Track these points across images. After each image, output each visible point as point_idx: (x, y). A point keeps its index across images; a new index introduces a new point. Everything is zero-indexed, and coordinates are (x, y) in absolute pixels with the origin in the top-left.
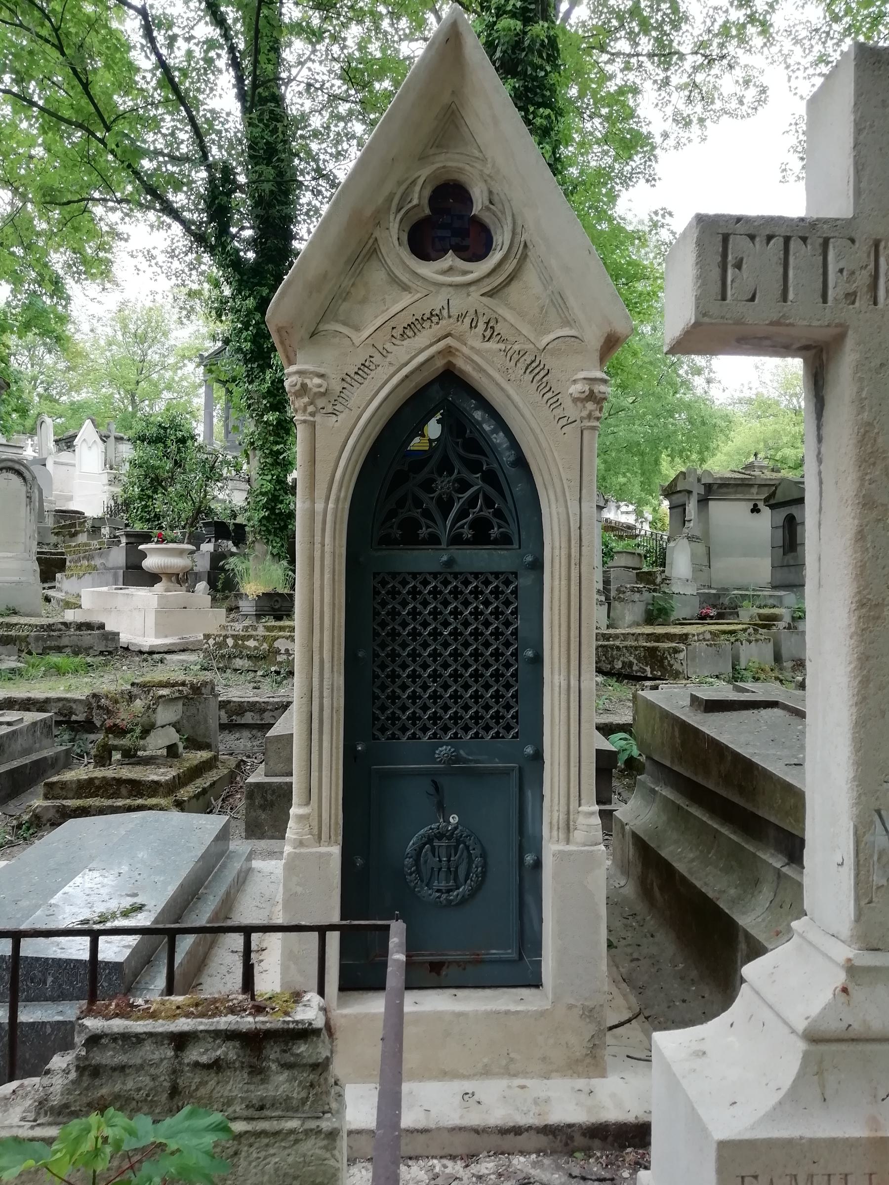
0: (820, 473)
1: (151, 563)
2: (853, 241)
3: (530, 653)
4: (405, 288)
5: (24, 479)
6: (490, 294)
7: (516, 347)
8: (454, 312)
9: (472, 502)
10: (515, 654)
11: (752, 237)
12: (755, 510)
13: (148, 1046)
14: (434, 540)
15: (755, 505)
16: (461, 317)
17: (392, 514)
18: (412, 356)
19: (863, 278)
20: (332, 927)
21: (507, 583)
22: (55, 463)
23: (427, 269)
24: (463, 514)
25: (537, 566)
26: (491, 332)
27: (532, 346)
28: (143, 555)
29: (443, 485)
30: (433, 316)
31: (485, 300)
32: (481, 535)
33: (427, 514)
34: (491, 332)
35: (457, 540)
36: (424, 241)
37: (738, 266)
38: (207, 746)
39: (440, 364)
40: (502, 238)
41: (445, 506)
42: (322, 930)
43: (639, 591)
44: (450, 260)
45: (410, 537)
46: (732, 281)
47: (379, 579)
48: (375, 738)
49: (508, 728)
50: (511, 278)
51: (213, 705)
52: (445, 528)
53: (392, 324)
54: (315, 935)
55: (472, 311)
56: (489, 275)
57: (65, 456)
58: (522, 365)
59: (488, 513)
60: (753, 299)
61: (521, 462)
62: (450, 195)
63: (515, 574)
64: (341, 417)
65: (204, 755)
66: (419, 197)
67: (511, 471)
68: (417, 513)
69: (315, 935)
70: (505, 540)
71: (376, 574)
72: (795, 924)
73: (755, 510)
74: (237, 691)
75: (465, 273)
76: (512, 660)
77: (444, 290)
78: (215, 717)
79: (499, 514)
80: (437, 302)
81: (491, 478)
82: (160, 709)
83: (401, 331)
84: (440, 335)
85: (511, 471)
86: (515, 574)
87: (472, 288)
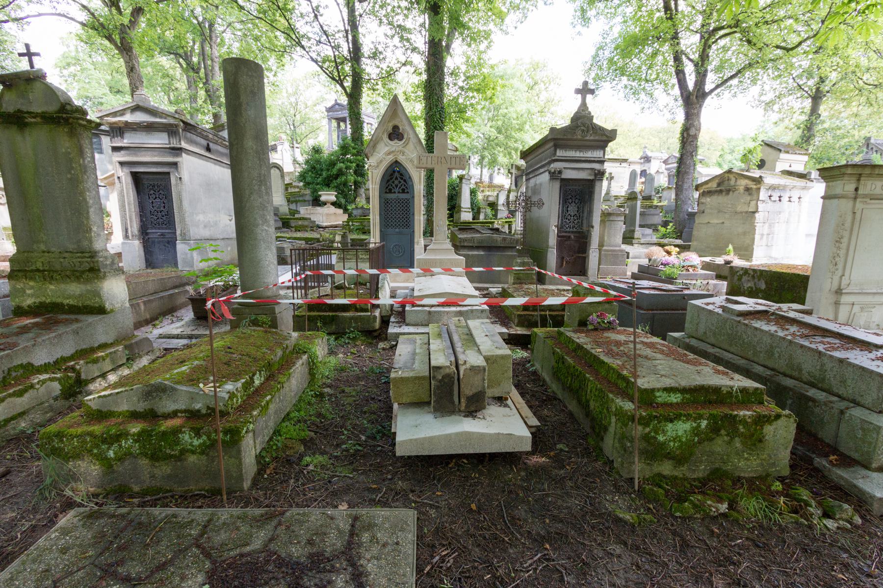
0: (34, 407)
1: (323, 198)
18: (390, 158)
23: (391, 143)
25: (413, 197)
26: (403, 154)
28: (320, 196)
29: (396, 182)
30: (393, 152)
32: (403, 191)
36: (391, 137)
40: (405, 136)
41: (397, 186)
43: (655, 54)
44: (396, 141)
45: (390, 192)
46: (546, 290)
52: (397, 190)
61: (410, 178)
62: (396, 128)
66: (390, 129)
80: (393, 149)
81: (405, 181)
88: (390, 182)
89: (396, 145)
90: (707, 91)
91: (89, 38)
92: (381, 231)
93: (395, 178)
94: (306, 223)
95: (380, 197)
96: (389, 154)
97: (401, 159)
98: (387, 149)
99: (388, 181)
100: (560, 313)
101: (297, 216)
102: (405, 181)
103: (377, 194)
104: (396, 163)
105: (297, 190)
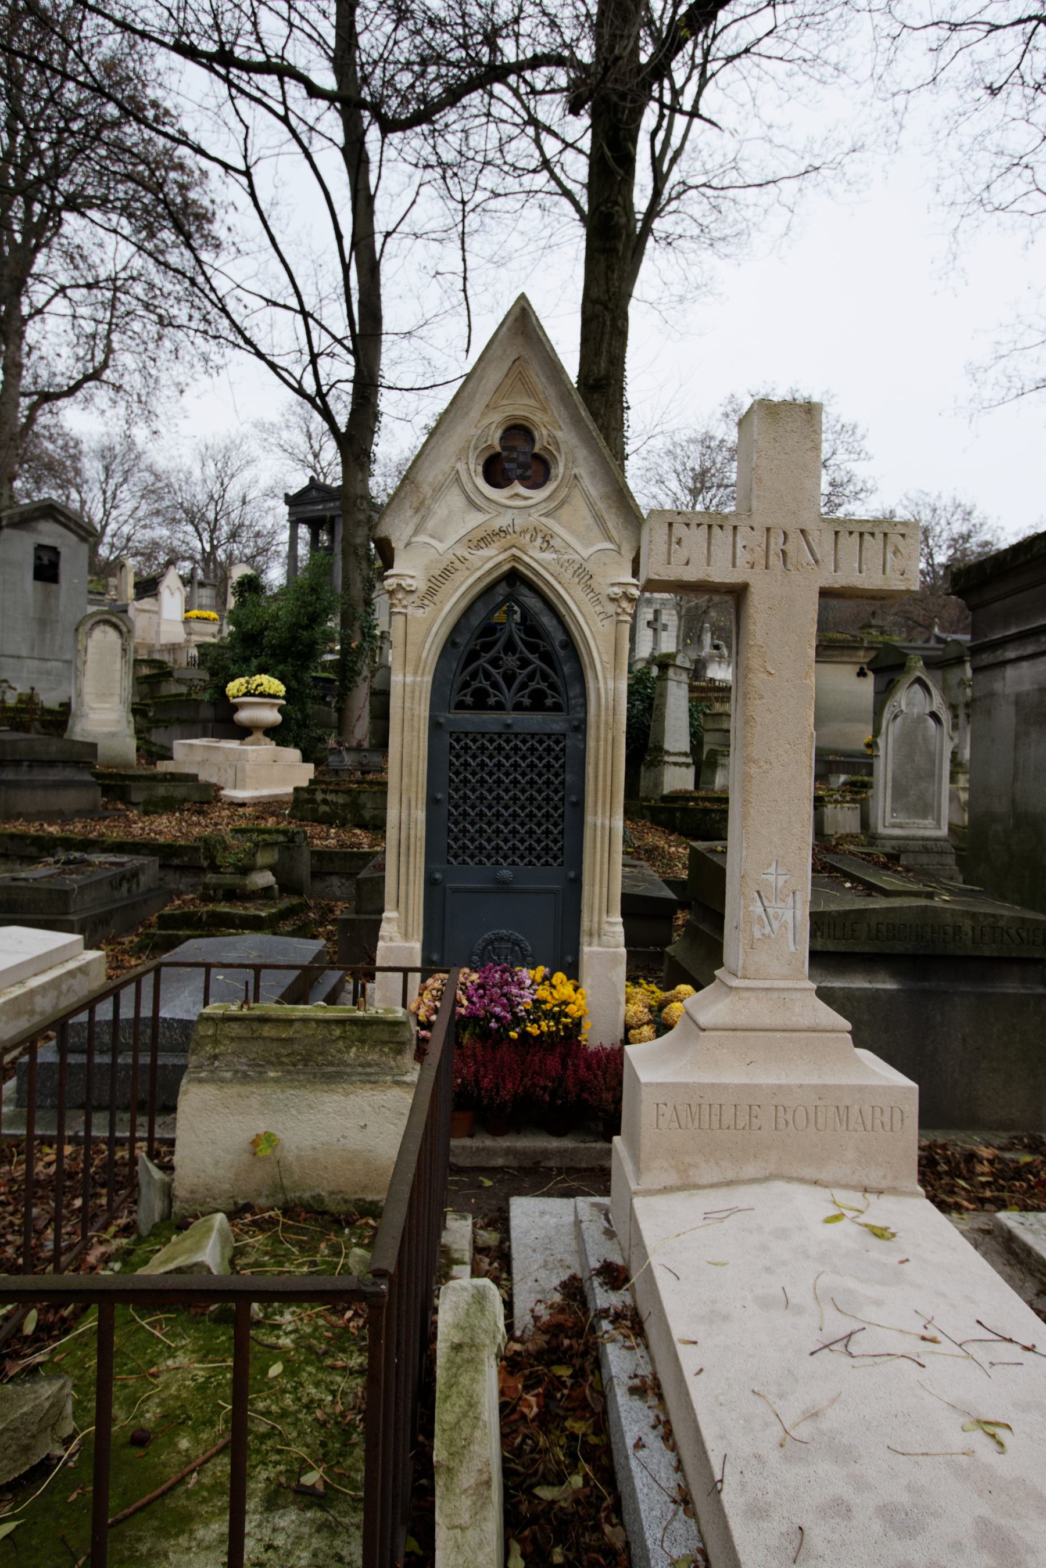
2: (752, 528)
3: (574, 799)
4: (479, 509)
5: (120, 632)
6: (546, 515)
7: (566, 557)
8: (517, 529)
9: (531, 677)
10: (562, 799)
11: (688, 525)
12: (861, 674)
13: (297, 1026)
14: (499, 706)
15: (862, 669)
16: (524, 532)
17: (466, 685)
18: (490, 559)
19: (760, 552)
20: (414, 970)
21: (557, 742)
22: (137, 610)
24: (523, 686)
25: (581, 728)
26: (547, 543)
27: (577, 557)
31: (543, 519)
32: (538, 703)
33: (495, 685)
34: (547, 543)
35: (518, 707)
36: (495, 471)
37: (679, 542)
38: (300, 893)
39: (506, 567)
42: (406, 971)
45: (480, 702)
47: (454, 736)
48: (449, 862)
49: (555, 858)
50: (562, 503)
51: (306, 856)
53: (468, 538)
54: (400, 975)
55: (531, 528)
56: (546, 500)
57: (147, 603)
58: (571, 571)
59: (543, 686)
60: (687, 563)
63: (564, 735)
64: (428, 609)
65: (295, 901)
67: (562, 653)
68: (486, 684)
69: (400, 975)
70: (557, 708)
71: (451, 733)
72: (716, 972)
73: (861, 674)
74: (329, 839)
75: (526, 498)
76: (560, 804)
77: (510, 511)
78: (304, 866)
79: (552, 686)
80: (503, 521)
81: (547, 657)
82: (258, 855)
83: (475, 542)
84: (507, 545)
85: (562, 653)
86: (564, 735)
87: (532, 510)
88: (483, 661)
89: (517, 504)
90: (382, 499)
91: (32, 1013)
92: (430, 882)
93: (513, 641)
94: (180, 792)
95: (435, 726)
96: (484, 541)
97: (538, 559)
98: (475, 519)
99: (473, 656)
100: (374, 917)
101: (163, 767)
102: (547, 657)
103: (423, 711)
104: (514, 580)
105: (184, 690)
